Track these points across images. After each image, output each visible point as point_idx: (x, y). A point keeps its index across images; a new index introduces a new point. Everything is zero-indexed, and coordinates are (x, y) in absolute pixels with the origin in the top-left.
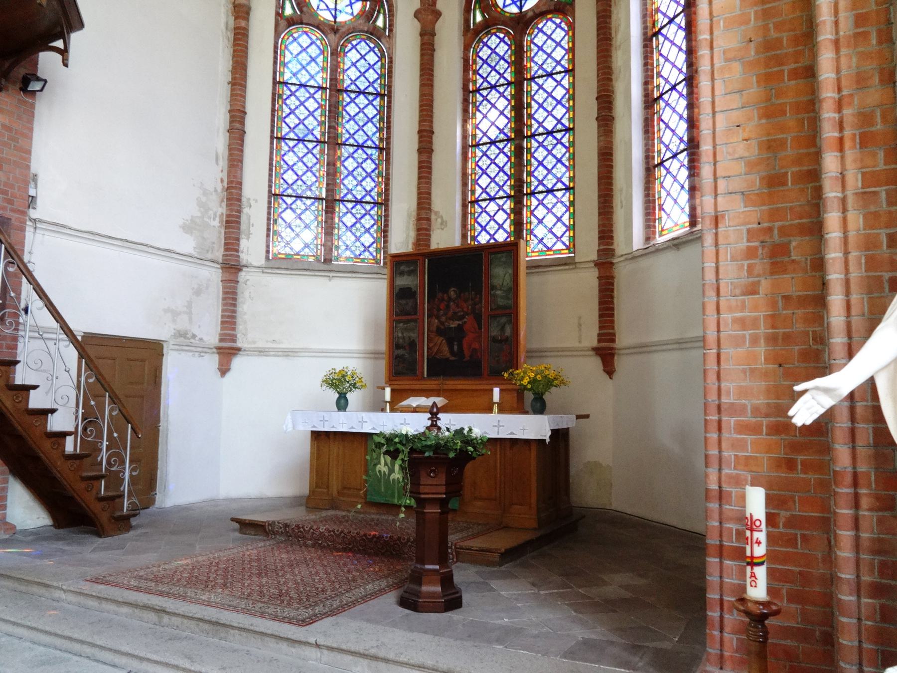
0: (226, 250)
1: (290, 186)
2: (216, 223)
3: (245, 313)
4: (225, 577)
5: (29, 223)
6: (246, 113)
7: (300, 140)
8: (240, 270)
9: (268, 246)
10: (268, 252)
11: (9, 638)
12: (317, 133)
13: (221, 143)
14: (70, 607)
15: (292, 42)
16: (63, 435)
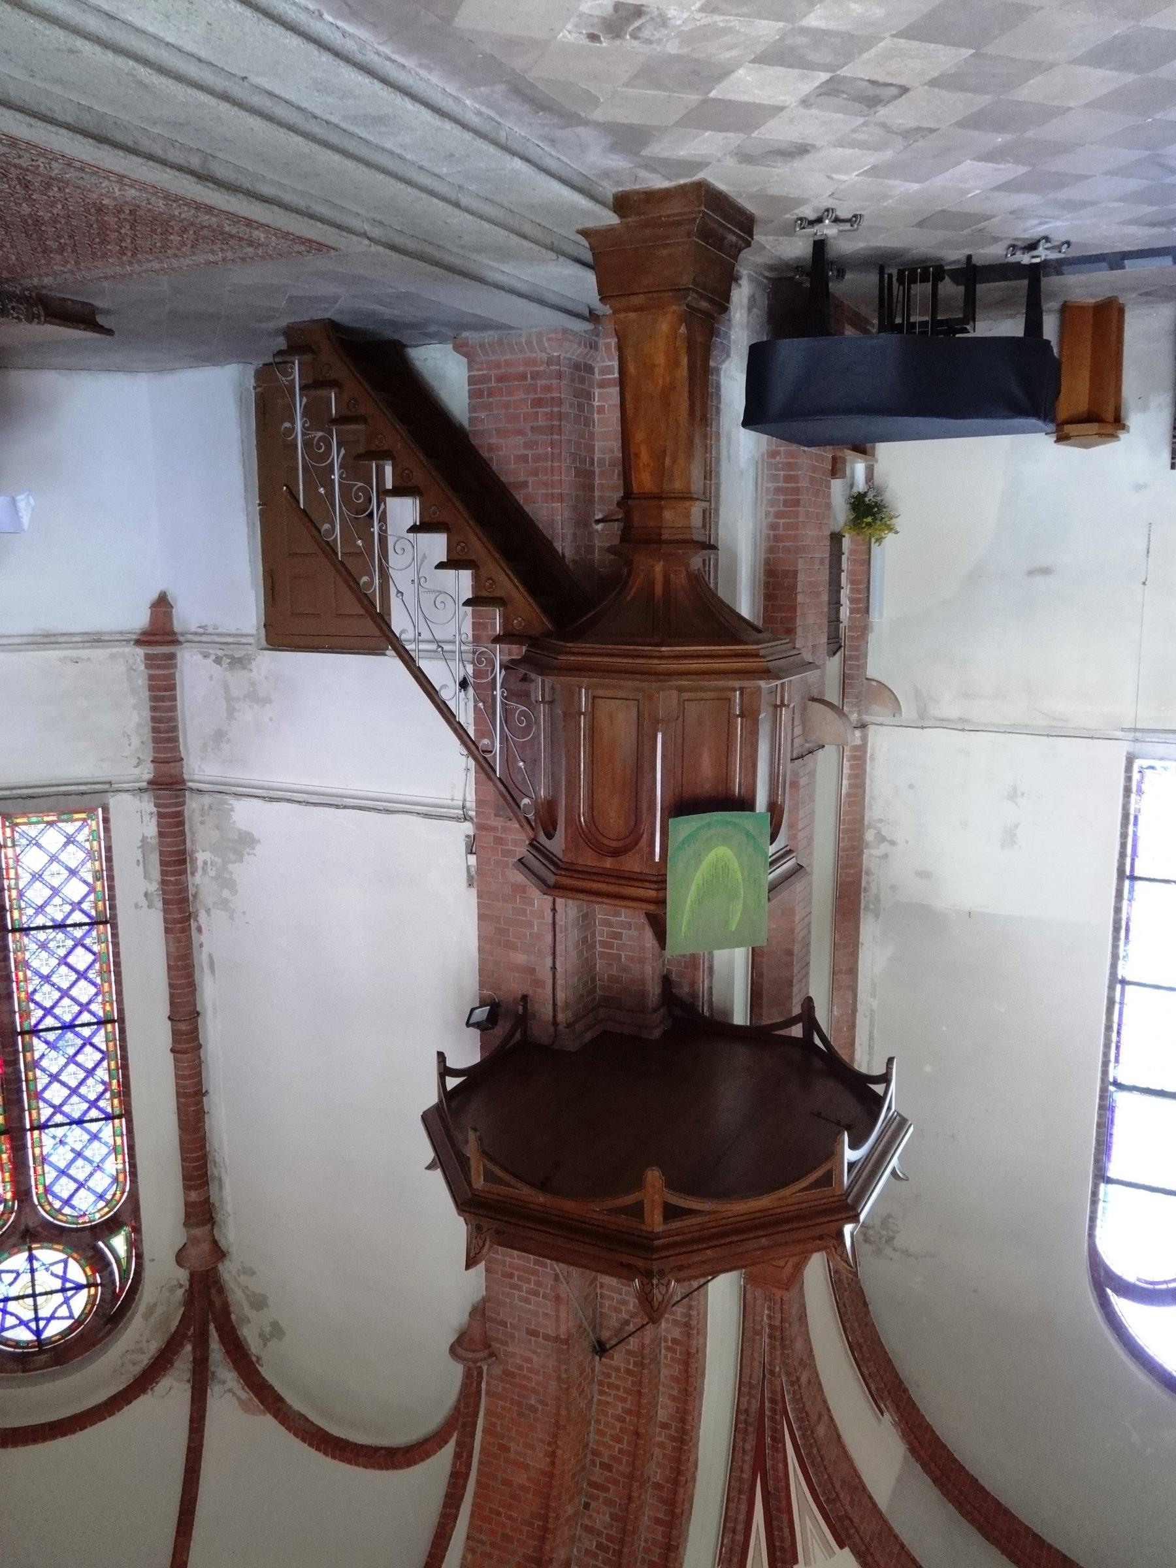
0: (180, 814)
1: (79, 943)
2: (201, 857)
3: (134, 707)
4: (103, 227)
5: (473, 814)
6: (172, 1050)
7: (69, 1027)
8: (150, 783)
9: (107, 830)
10: (106, 820)
11: (436, 170)
12: (39, 1046)
13: (210, 991)
14: (355, 209)
15: (106, 1191)
16: (398, 491)
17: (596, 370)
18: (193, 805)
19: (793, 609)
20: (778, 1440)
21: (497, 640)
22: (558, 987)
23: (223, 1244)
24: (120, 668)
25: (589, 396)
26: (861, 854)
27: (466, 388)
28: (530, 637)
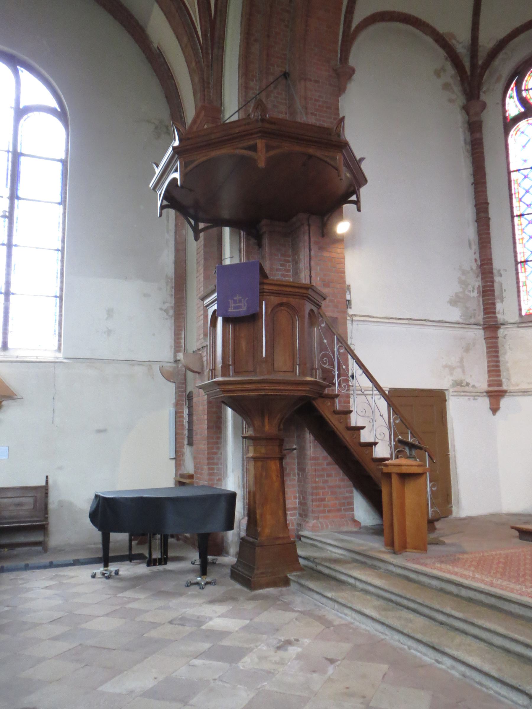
2: (475, 294)
5: (348, 318)
13: (471, 232)
17: (298, 515)
18: (480, 317)
19: (208, 412)
20: (204, 35)
21: (337, 396)
22: (308, 241)
23: (464, 111)
24: (514, 380)
25: (301, 503)
26: (175, 304)
27: (355, 506)
28: (323, 397)
